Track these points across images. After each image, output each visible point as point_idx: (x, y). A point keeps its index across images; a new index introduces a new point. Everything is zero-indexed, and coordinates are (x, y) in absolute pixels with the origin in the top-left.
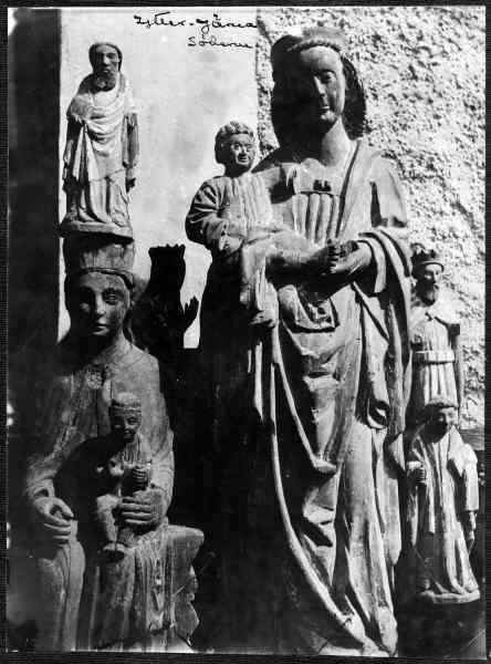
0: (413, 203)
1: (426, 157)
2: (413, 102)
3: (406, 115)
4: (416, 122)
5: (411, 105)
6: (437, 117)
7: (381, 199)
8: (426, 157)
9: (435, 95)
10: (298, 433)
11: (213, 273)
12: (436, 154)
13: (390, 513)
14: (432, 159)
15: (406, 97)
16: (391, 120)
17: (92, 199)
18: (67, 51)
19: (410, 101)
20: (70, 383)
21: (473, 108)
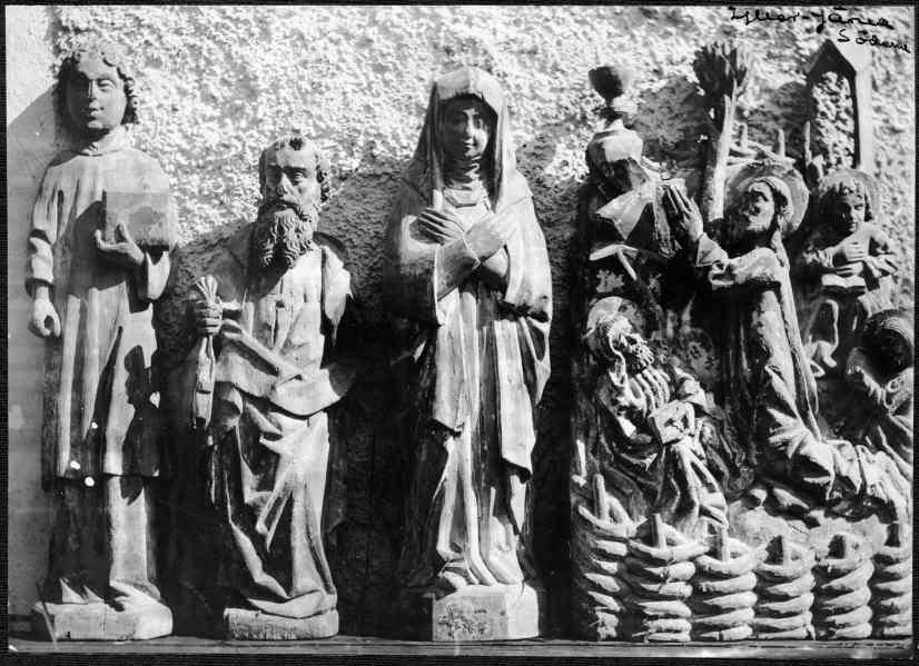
0: (342, 224)
1: (361, 141)
2: (337, 43)
3: (322, 67)
4: (341, 79)
5: (331, 47)
6: (380, 69)
7: (863, 465)
8: (361, 141)
9: (375, 29)
10: (201, 635)
11: (431, 575)
12: (379, 135)
13: (68, 462)
14: (371, 145)
15: (324, 34)
16: (294, 76)
17: (618, 544)
18: (290, 15)
19: (331, 41)
20: (71, 459)
21: (448, 51)
